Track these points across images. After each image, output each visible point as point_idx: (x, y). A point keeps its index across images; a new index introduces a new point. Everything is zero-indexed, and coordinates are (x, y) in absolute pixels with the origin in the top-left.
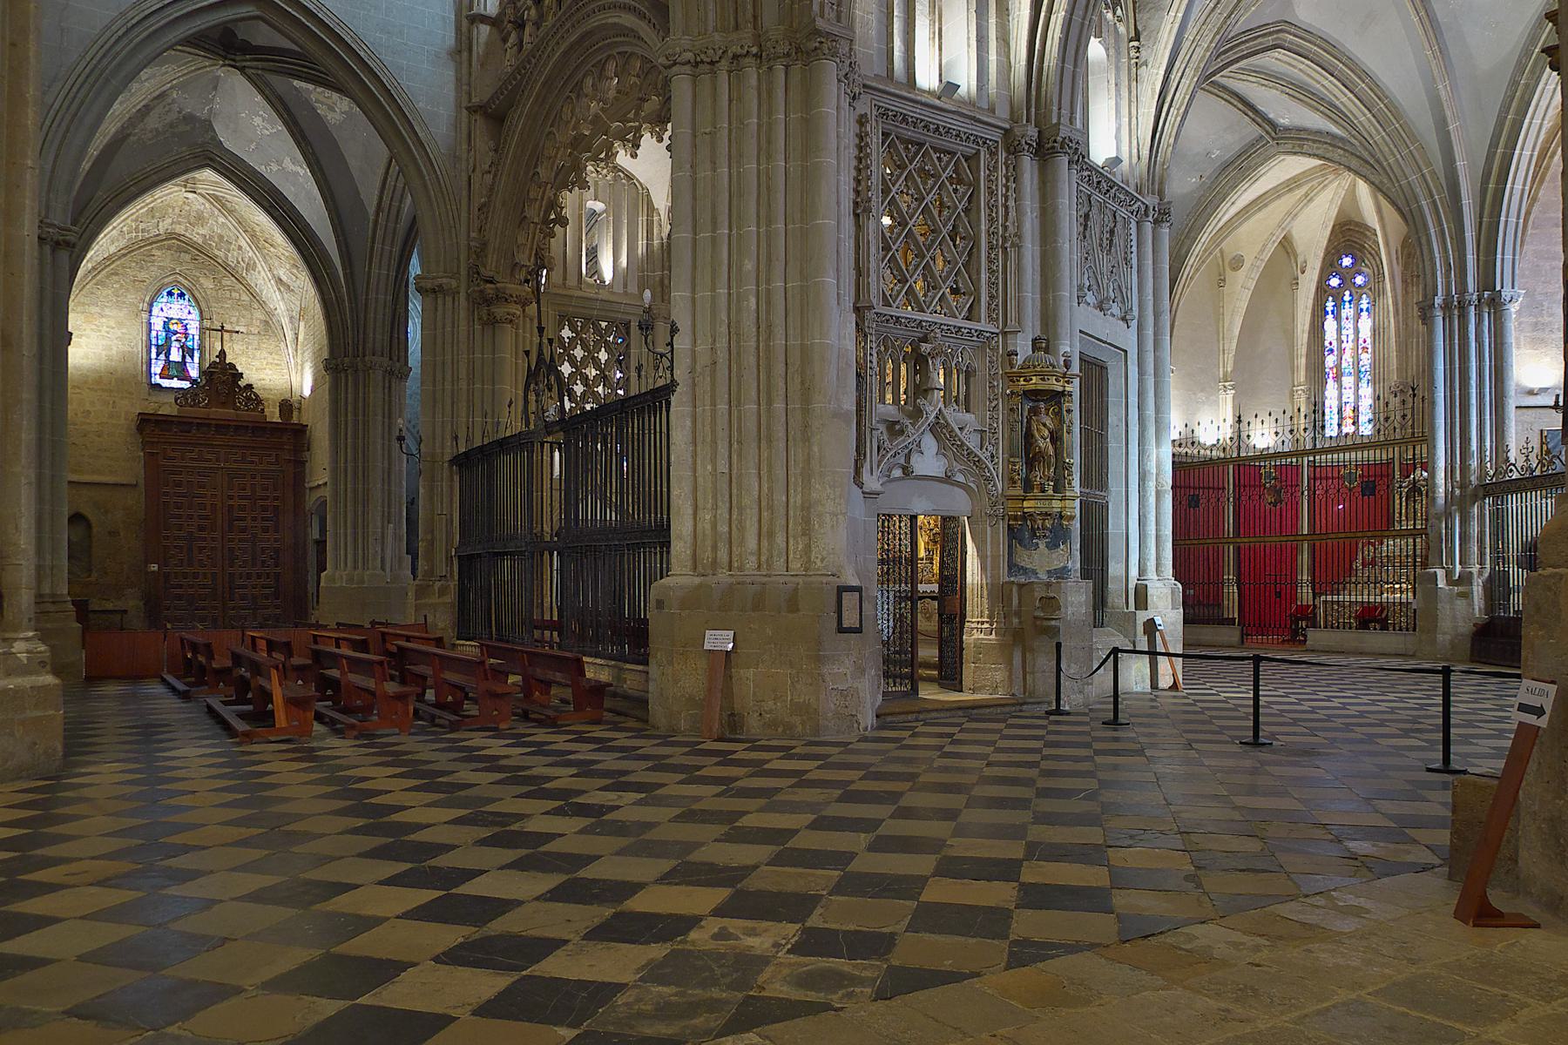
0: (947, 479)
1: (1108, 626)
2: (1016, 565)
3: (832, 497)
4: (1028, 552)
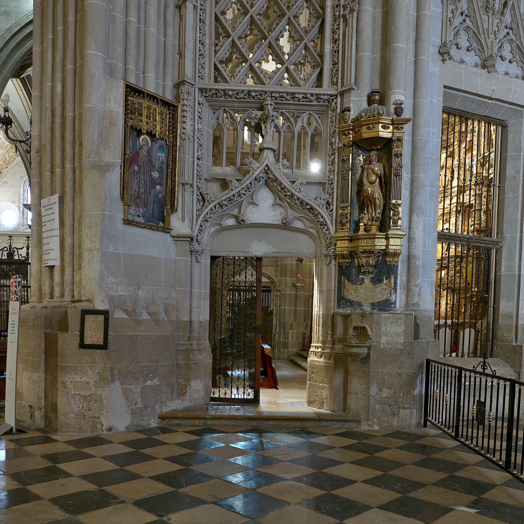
0: (285, 226)
1: (497, 357)
2: (343, 298)
3: (89, 236)
4: (354, 287)
